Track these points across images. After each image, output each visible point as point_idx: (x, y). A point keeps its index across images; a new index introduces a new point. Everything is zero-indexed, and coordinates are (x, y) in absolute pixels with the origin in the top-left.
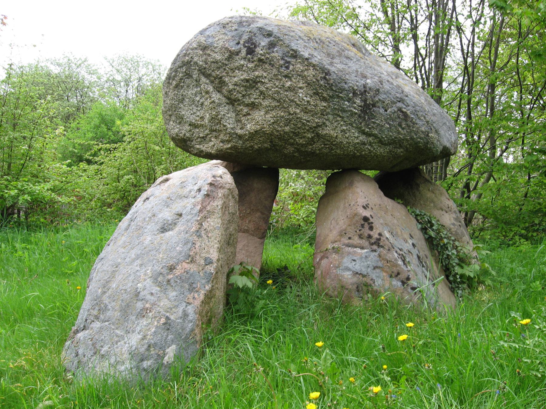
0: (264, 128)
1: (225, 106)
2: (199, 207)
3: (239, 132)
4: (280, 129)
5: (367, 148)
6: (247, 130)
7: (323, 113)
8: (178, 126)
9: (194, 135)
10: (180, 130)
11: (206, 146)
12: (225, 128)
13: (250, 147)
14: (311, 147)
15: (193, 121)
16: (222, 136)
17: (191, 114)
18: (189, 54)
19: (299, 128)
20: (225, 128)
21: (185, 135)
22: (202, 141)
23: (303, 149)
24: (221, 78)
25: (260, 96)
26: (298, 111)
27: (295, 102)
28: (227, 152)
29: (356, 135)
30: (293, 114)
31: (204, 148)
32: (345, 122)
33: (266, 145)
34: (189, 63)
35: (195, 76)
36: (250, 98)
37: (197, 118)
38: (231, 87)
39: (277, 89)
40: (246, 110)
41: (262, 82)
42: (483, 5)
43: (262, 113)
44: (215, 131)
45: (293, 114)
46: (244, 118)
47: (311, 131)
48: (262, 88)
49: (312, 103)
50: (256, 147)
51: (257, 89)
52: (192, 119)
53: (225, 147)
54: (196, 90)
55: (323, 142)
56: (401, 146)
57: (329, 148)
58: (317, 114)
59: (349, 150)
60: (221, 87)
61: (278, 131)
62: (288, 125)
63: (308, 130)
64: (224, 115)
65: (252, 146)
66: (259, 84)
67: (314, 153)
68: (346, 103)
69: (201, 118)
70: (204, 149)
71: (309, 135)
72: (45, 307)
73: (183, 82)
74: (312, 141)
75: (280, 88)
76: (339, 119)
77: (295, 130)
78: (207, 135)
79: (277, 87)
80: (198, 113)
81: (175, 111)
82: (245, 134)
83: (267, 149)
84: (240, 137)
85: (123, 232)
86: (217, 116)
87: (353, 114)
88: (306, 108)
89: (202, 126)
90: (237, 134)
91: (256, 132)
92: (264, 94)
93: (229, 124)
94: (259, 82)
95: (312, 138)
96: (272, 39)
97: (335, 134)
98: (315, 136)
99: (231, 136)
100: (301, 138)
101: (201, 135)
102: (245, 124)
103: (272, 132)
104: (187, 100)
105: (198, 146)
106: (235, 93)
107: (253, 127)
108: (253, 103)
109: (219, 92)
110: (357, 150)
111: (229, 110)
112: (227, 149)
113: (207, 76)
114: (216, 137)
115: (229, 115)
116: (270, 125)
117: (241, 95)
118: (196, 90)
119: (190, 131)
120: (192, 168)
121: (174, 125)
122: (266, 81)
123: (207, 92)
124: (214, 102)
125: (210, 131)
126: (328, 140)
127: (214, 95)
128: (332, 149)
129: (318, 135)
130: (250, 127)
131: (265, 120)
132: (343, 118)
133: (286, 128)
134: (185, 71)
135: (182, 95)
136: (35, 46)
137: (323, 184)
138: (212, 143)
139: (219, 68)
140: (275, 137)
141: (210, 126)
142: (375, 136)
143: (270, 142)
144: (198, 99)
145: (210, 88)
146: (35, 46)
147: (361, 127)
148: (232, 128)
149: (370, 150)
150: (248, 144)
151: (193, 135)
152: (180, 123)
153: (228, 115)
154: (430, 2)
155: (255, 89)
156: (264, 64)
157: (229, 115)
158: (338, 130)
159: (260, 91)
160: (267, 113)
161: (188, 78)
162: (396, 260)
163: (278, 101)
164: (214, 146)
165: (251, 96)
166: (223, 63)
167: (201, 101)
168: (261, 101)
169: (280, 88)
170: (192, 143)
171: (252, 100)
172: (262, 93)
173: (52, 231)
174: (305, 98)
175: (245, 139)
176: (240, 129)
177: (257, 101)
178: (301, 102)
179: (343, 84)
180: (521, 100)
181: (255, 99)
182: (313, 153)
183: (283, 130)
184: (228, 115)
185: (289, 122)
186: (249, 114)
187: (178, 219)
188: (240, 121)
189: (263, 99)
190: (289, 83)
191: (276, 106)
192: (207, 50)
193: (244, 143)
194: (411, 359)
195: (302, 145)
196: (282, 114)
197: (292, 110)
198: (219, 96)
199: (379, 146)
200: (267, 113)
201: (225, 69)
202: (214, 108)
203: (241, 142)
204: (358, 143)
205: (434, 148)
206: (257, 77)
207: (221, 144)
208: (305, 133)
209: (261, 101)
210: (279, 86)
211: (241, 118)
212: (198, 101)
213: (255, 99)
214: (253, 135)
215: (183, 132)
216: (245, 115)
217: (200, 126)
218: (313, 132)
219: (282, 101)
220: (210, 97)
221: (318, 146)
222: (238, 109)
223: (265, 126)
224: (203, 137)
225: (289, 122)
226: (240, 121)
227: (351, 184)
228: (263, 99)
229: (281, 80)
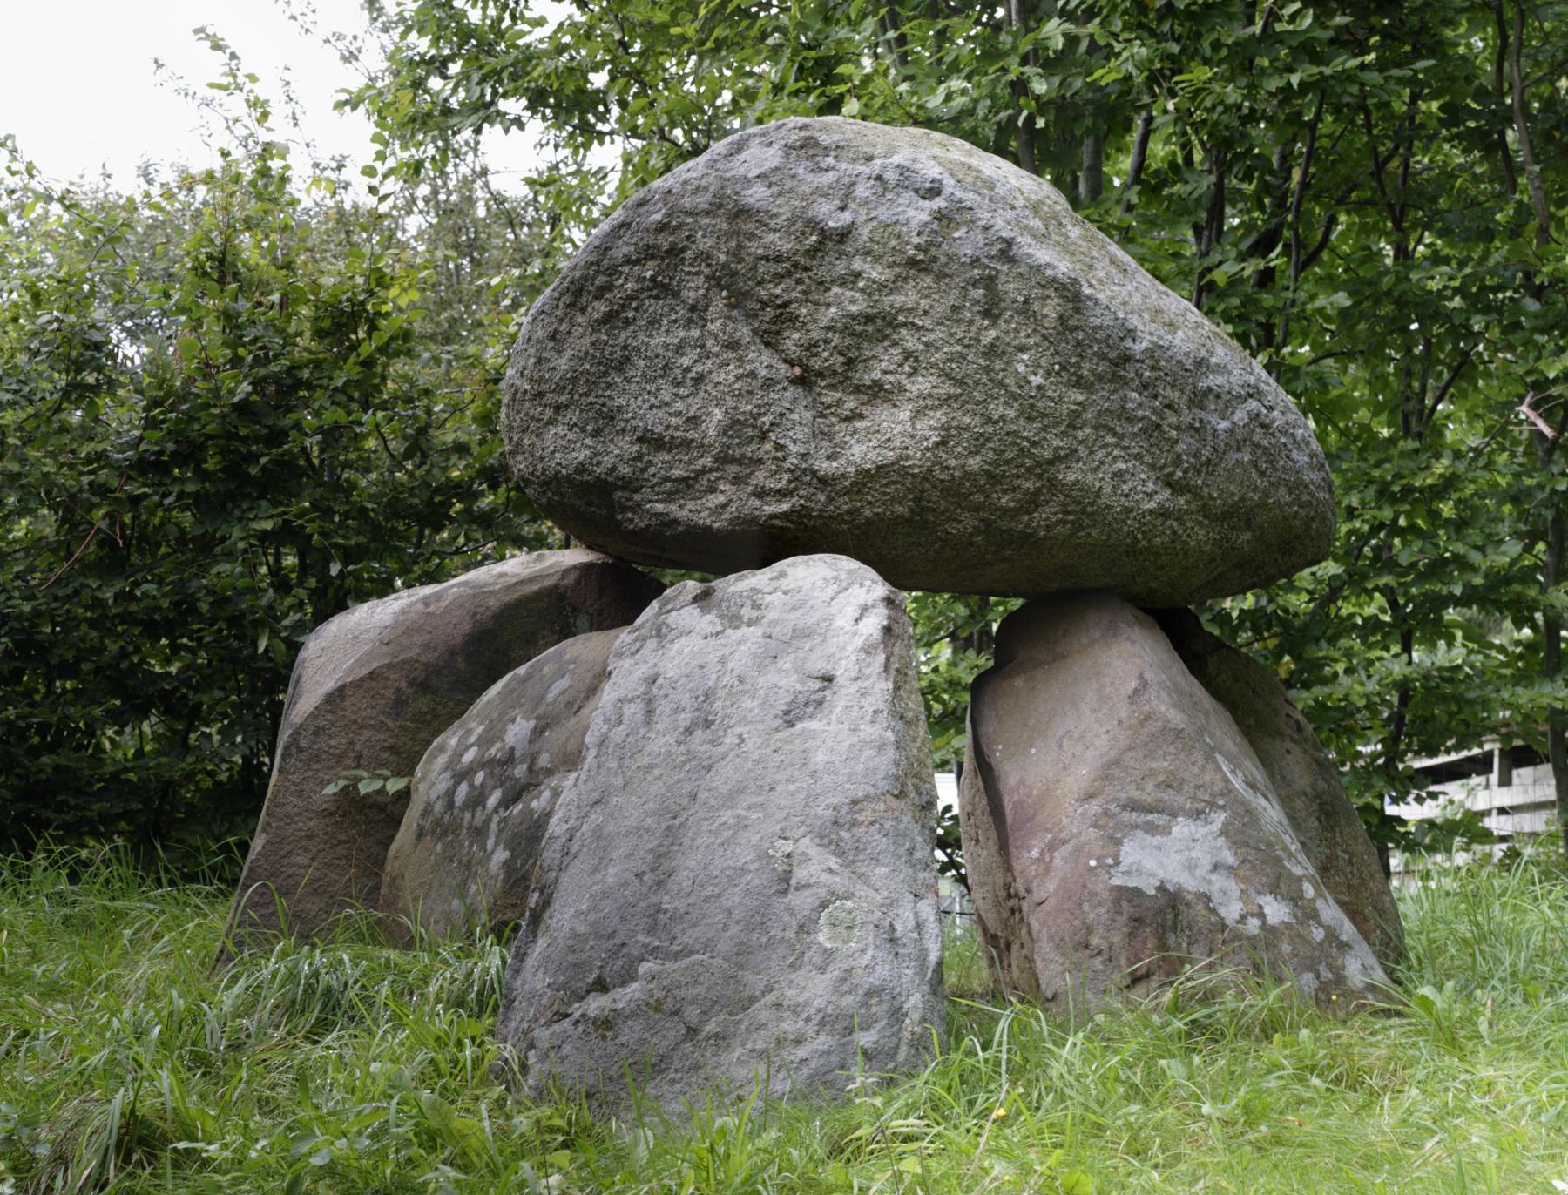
0: (907, 458)
1: (785, 389)
2: (567, 299)
3: (825, 467)
4: (953, 463)
5: (1171, 527)
6: (849, 463)
7: (1074, 422)
8: (588, 441)
9: (652, 470)
10: (596, 454)
11: (691, 505)
12: (780, 455)
13: (848, 512)
14: (1026, 518)
15: (658, 429)
16: (760, 478)
17: (652, 407)
18: (680, 226)
19: (1007, 462)
20: (780, 455)
21: (614, 468)
22: (677, 491)
23: (1003, 525)
24: (786, 305)
25: (901, 365)
26: (1012, 413)
27: (1005, 386)
28: (773, 526)
29: (1150, 487)
30: (996, 422)
31: (684, 512)
32: (1125, 448)
33: (898, 509)
34: (675, 252)
35: (692, 294)
36: (869, 369)
37: (674, 421)
38: (816, 335)
39: (959, 348)
40: (852, 405)
41: (913, 324)
42: (934, 408)
43: (904, 414)
44: (738, 461)
45: (996, 422)
46: (844, 425)
47: (1038, 471)
48: (912, 343)
49: (1049, 393)
50: (867, 513)
51: (895, 344)
52: (655, 420)
53: (768, 509)
54: (682, 334)
55: (1065, 505)
56: (1248, 525)
57: (1073, 522)
58: (1058, 424)
59: (1125, 529)
60: (777, 333)
61: (947, 468)
62: (977, 453)
63: (1029, 470)
64: (782, 415)
65: (854, 512)
66: (903, 331)
67: (1032, 535)
68: (1134, 395)
69: (688, 419)
70: (682, 514)
71: (1029, 485)
72: (175, 1150)
73: (636, 309)
74: (1032, 502)
75: (967, 346)
76: (1110, 439)
77: (997, 467)
78: (703, 472)
79: (959, 341)
80: (679, 406)
81: (586, 395)
82: (843, 475)
83: (898, 520)
84: (824, 482)
85: (642, 731)
86: (756, 417)
87: (379, 258)
88: (1032, 406)
89: (686, 444)
90: (814, 473)
91: (879, 468)
92: (917, 360)
93: (794, 442)
94: (904, 324)
95: (1038, 490)
96: (939, 203)
97: (1097, 484)
98: (1043, 486)
99: (796, 479)
100: (1005, 492)
101: (677, 473)
102: (843, 445)
103: (930, 471)
104: (642, 363)
105: (659, 507)
106: (826, 354)
107: (872, 455)
108: (877, 384)
109: (767, 344)
110: (1144, 533)
111: (795, 400)
112: (774, 516)
113: (738, 300)
114: (736, 481)
115: (796, 417)
116: (927, 449)
117: (842, 359)
118: (682, 334)
119: (639, 457)
120: (570, 641)
121: (571, 436)
122: (928, 323)
123: (732, 345)
124: (752, 374)
125: (716, 460)
126: (1083, 506)
127: (752, 355)
128: (1081, 528)
129: (1053, 485)
130: (860, 452)
131: (913, 437)
132: (1121, 437)
133: (971, 461)
134: (653, 278)
135: (625, 348)
136: (159, 66)
137: (874, 582)
138: (722, 499)
139: (778, 278)
140: (935, 487)
141: (723, 444)
142: (1195, 492)
143: (914, 500)
144: (685, 361)
145: (744, 333)
146: (159, 66)
147: (681, 79)
148: (803, 455)
149: (1175, 533)
150: (844, 504)
151: (644, 470)
152: (597, 433)
153: (792, 416)
154: (811, 4)
155: (886, 343)
156: (922, 275)
157: (796, 417)
158: (1105, 474)
159: (905, 351)
160: (917, 414)
161: (657, 298)
162: (1480, 745)
163: (960, 383)
164: (724, 506)
165: (875, 363)
166: (796, 265)
167: (699, 368)
168: (903, 379)
169: (967, 346)
170: (637, 497)
171: (876, 375)
172: (908, 355)
173: (275, 936)
174: (1032, 378)
175: (839, 488)
176: (828, 457)
177: (891, 378)
178: (1021, 387)
179: (1128, 343)
180: (1147, 976)
181: (886, 372)
182: (1027, 538)
183: (963, 466)
184: (792, 416)
185: (983, 445)
186: (861, 417)
187: (823, 689)
188: (828, 436)
189: (909, 375)
190: (993, 333)
191: (949, 397)
192: (745, 221)
193: (830, 500)
194: (1078, 1065)
195: (1005, 511)
196: (967, 420)
197: (997, 409)
198: (767, 357)
199: (1200, 523)
200: (917, 414)
201: (799, 282)
202: (750, 393)
203: (823, 498)
204: (1151, 512)
205: (1032, 502)
206: (900, 310)
207: (757, 503)
208: (1018, 477)
209: (903, 379)
210: (966, 341)
211: (833, 425)
212: (688, 370)
213: (886, 372)
214: (867, 478)
215: (608, 461)
216: (848, 419)
217: (681, 444)
218: (1040, 476)
219: (970, 382)
220: (740, 359)
221: (1046, 514)
222: (827, 400)
223: (910, 452)
224: (684, 480)
225: (983, 445)
226: (828, 436)
227: (1112, 631)
228: (909, 375)
229: (971, 322)
